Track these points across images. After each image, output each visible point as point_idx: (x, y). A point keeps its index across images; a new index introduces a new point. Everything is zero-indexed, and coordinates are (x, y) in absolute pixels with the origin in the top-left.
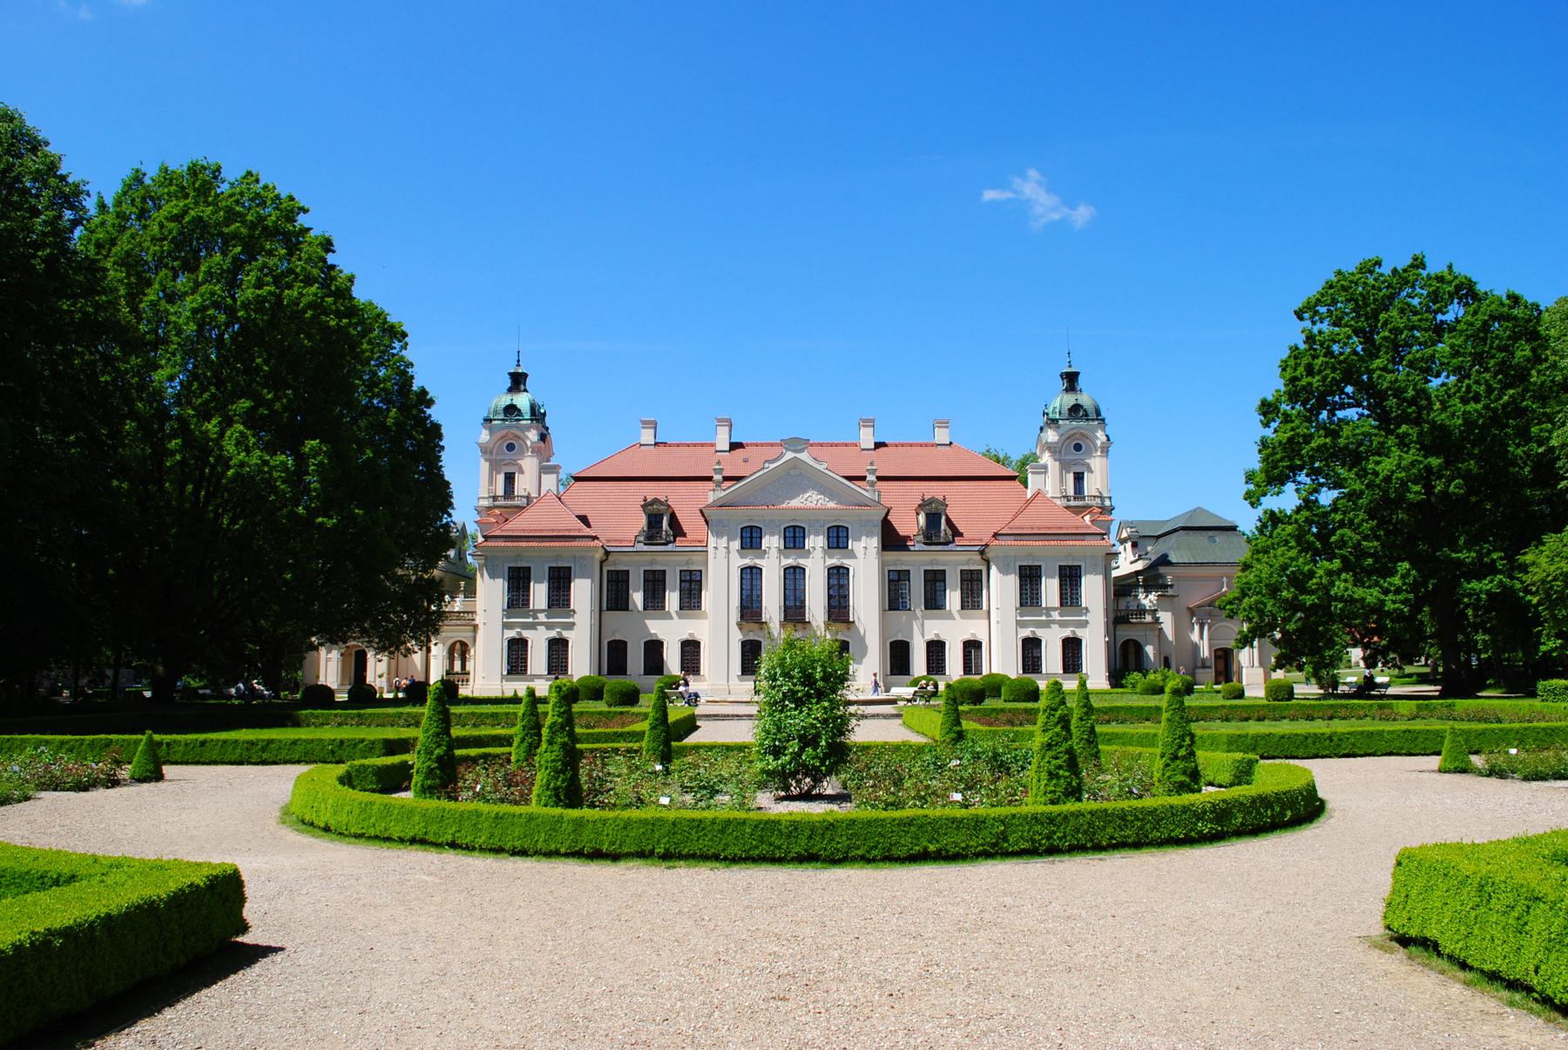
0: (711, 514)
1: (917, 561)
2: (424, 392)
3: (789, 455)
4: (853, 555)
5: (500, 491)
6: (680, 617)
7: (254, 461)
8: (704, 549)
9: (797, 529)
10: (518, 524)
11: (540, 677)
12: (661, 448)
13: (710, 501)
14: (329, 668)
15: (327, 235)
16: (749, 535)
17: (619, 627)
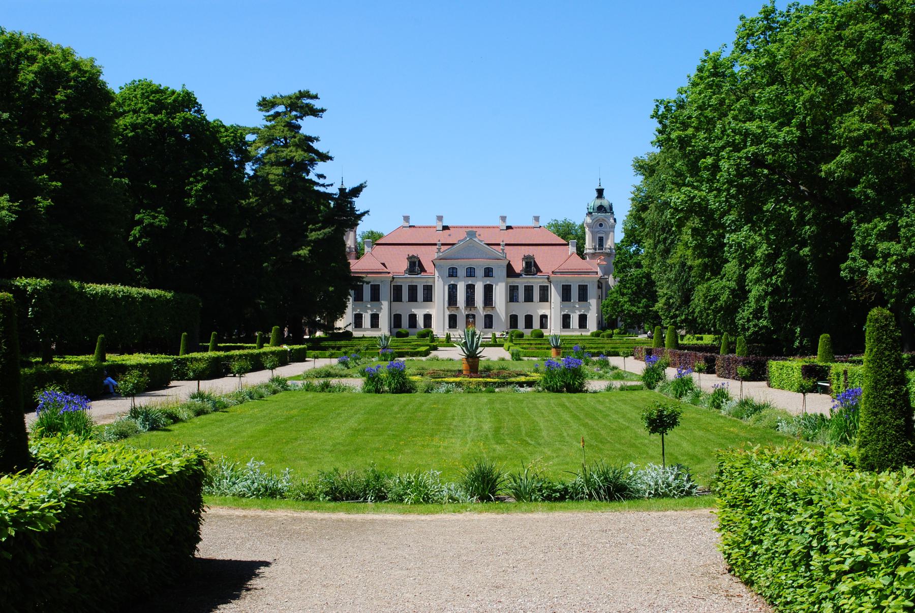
0: (437, 262)
1: (521, 283)
12: (412, 228)
15: (103, 70)
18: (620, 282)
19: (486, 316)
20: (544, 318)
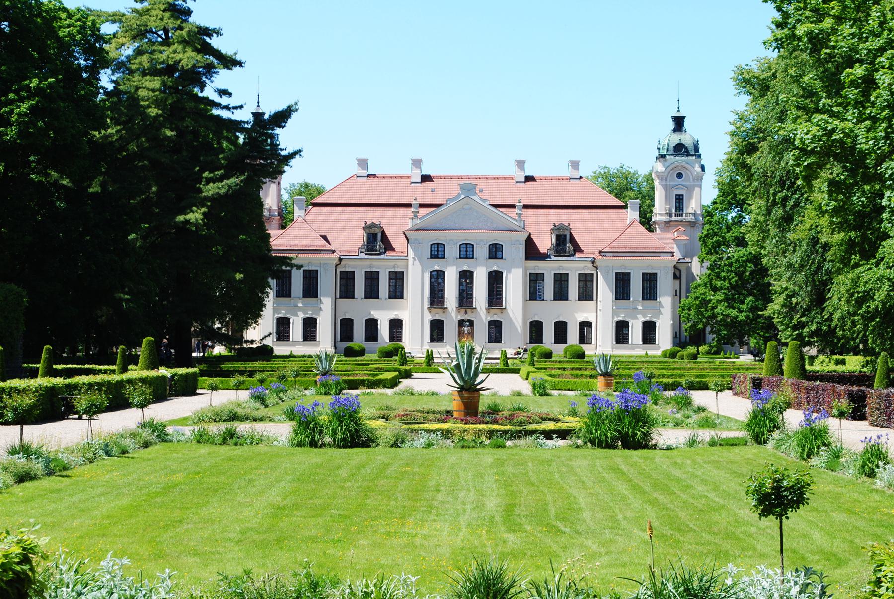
0: (412, 235)
8: (406, 258)
9: (468, 246)
12: (372, 180)
13: (410, 226)
16: (436, 249)
20: (585, 326)
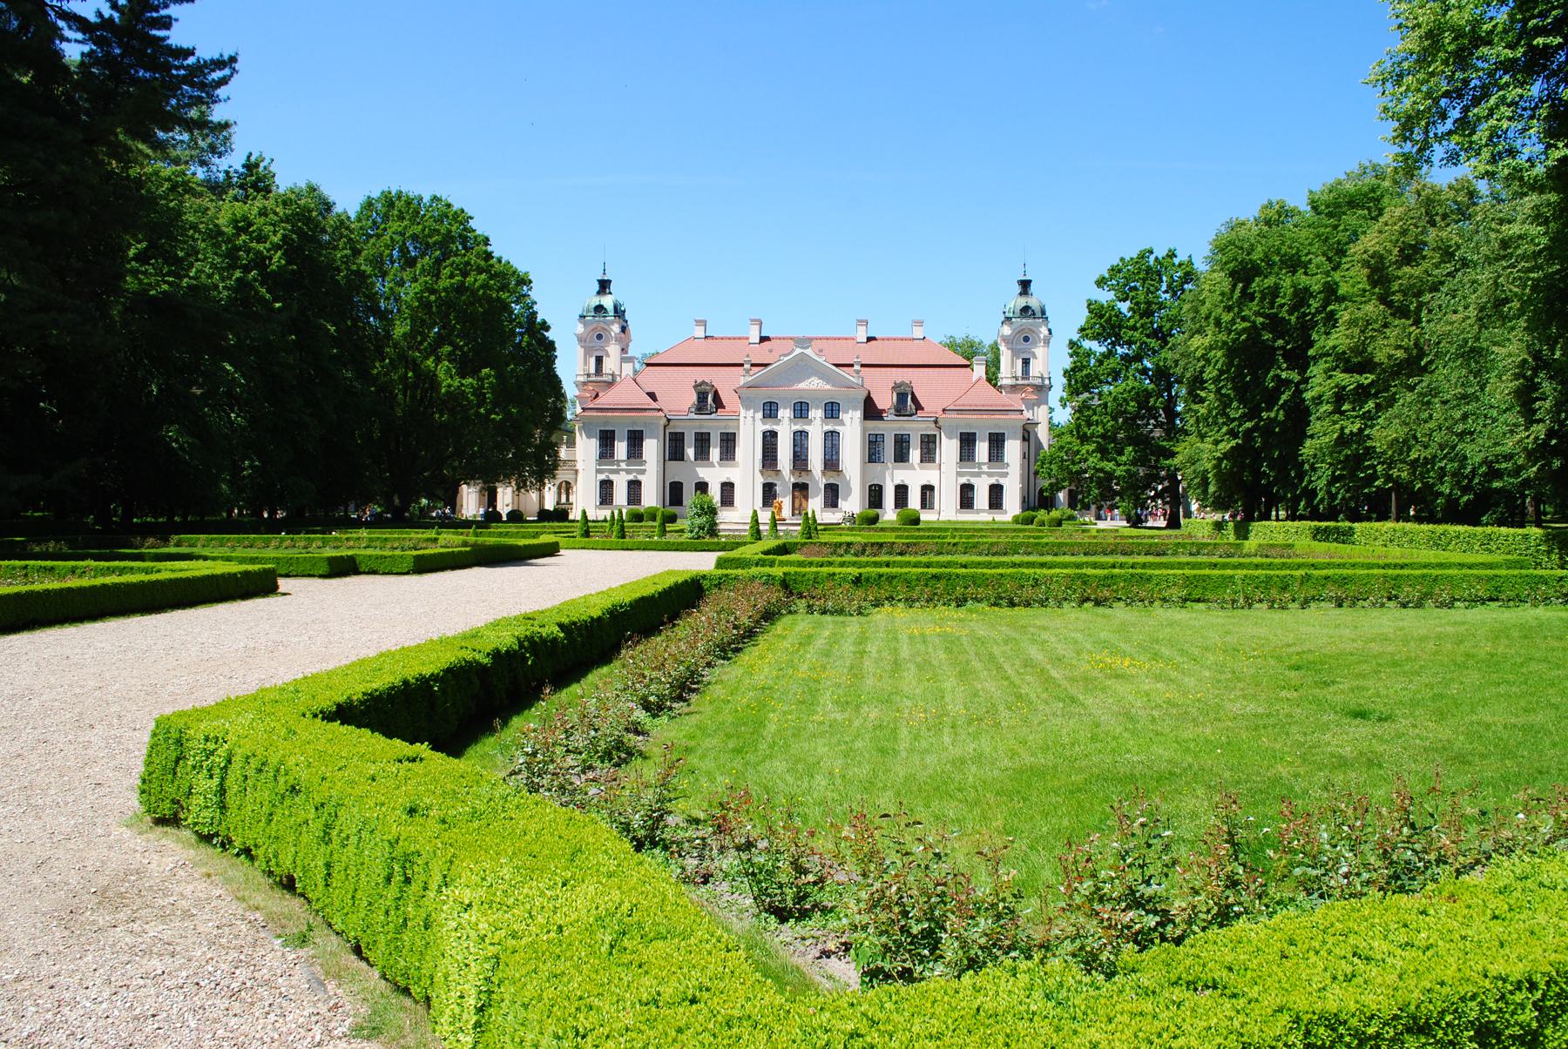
2: (544, 322)
3: (798, 351)
4: (842, 423)
5: (593, 370)
6: (720, 466)
7: (456, 384)
10: (607, 399)
11: (983, 511)
12: (710, 341)
14: (470, 502)
17: (677, 471)
18: (1080, 410)
19: (795, 486)
20: (927, 490)
